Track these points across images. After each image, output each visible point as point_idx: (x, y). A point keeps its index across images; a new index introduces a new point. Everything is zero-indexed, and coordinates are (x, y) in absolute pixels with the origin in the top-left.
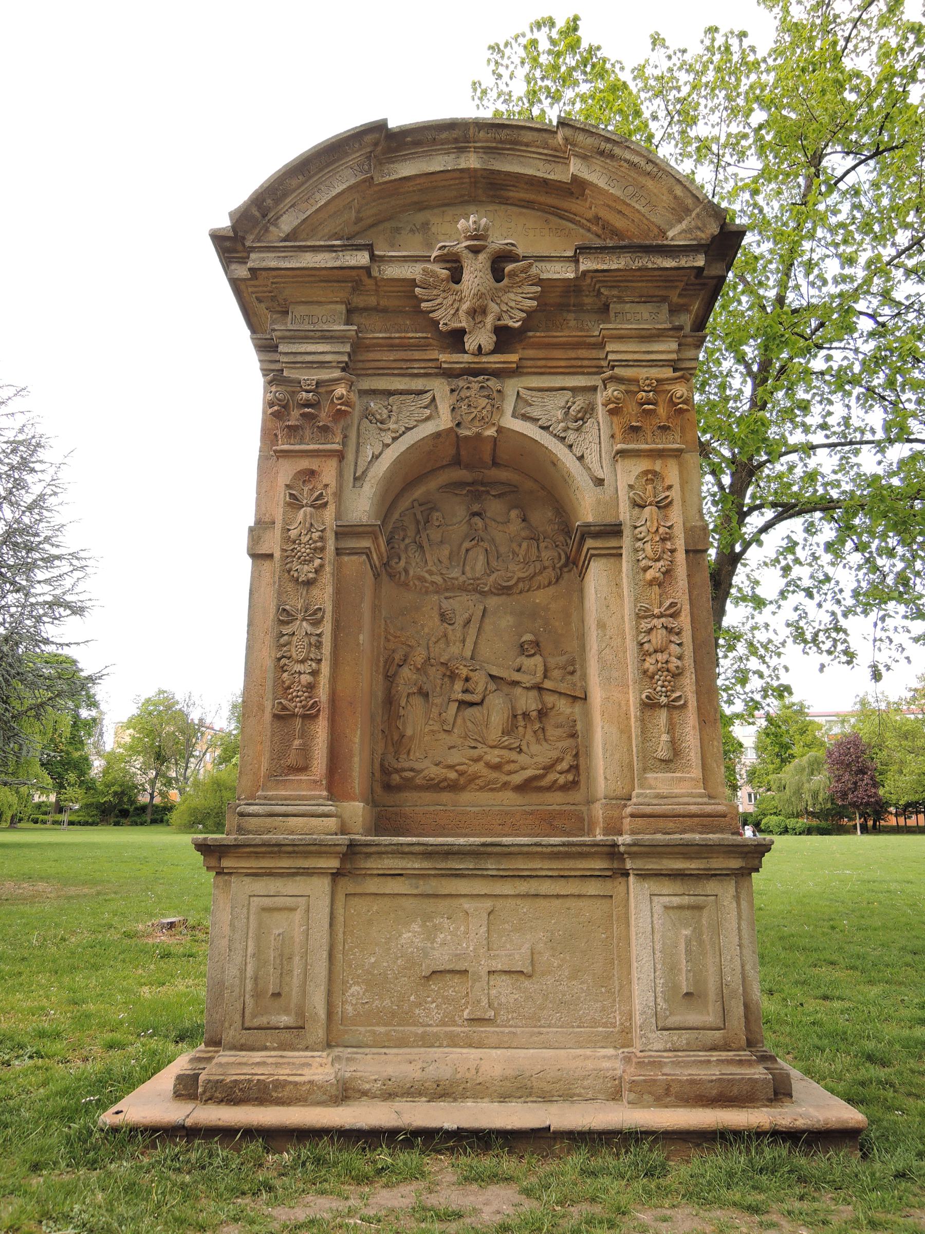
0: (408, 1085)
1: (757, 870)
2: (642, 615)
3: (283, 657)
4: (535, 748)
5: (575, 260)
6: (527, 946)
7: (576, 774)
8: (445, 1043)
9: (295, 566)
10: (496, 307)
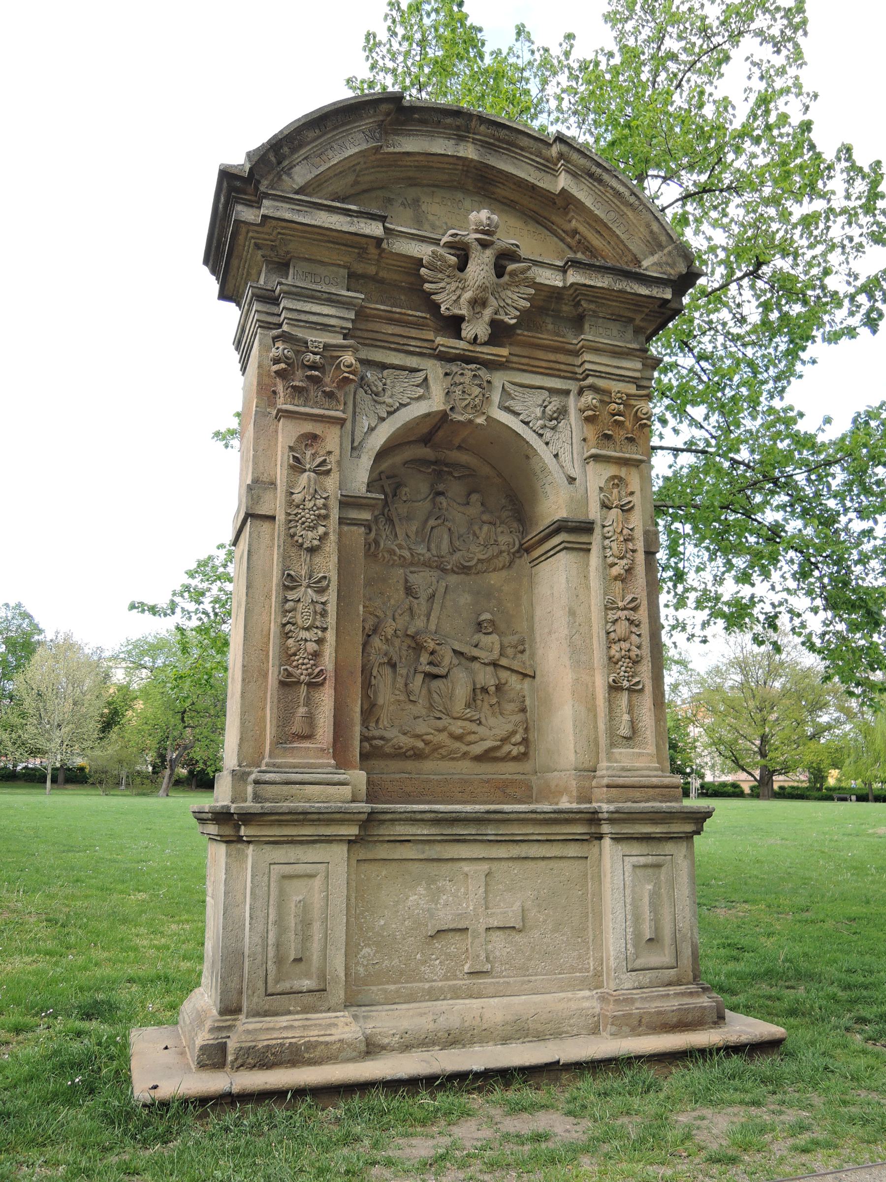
0: (423, 1036)
2: (610, 606)
3: (289, 623)
4: (492, 721)
5: (563, 270)
6: (518, 904)
7: (523, 747)
8: (449, 996)
9: (299, 531)
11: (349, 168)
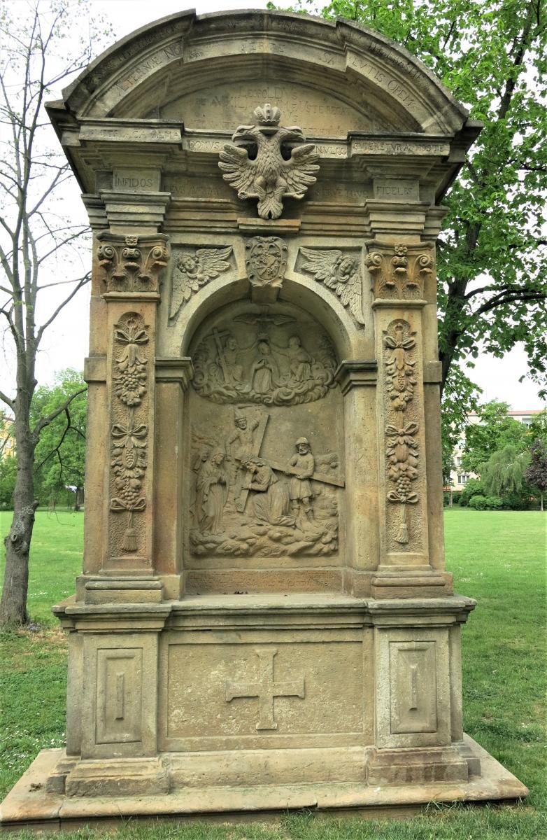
1: (464, 622)
3: (116, 465)
4: (306, 525)
6: (302, 677)
9: (124, 392)
10: (284, 181)
11: (159, 82)
